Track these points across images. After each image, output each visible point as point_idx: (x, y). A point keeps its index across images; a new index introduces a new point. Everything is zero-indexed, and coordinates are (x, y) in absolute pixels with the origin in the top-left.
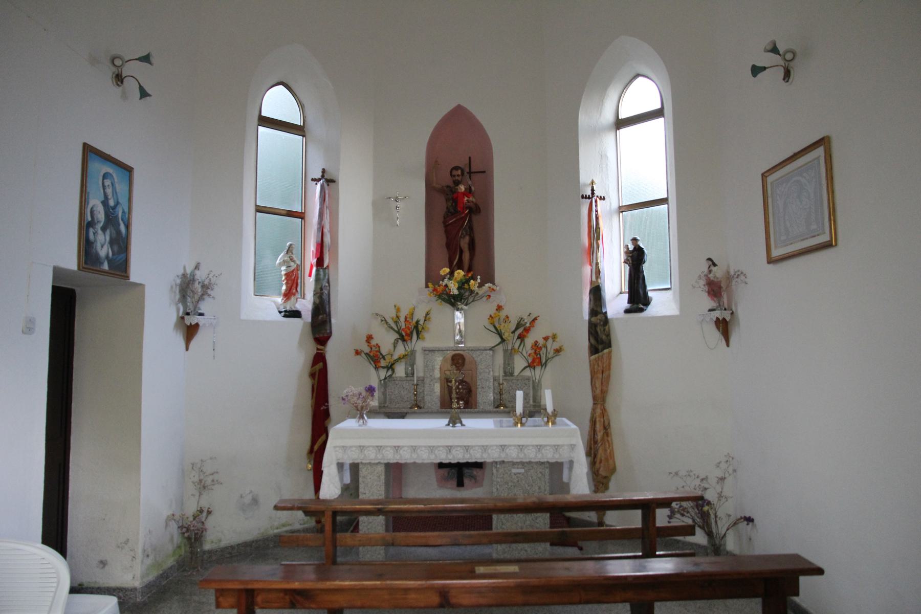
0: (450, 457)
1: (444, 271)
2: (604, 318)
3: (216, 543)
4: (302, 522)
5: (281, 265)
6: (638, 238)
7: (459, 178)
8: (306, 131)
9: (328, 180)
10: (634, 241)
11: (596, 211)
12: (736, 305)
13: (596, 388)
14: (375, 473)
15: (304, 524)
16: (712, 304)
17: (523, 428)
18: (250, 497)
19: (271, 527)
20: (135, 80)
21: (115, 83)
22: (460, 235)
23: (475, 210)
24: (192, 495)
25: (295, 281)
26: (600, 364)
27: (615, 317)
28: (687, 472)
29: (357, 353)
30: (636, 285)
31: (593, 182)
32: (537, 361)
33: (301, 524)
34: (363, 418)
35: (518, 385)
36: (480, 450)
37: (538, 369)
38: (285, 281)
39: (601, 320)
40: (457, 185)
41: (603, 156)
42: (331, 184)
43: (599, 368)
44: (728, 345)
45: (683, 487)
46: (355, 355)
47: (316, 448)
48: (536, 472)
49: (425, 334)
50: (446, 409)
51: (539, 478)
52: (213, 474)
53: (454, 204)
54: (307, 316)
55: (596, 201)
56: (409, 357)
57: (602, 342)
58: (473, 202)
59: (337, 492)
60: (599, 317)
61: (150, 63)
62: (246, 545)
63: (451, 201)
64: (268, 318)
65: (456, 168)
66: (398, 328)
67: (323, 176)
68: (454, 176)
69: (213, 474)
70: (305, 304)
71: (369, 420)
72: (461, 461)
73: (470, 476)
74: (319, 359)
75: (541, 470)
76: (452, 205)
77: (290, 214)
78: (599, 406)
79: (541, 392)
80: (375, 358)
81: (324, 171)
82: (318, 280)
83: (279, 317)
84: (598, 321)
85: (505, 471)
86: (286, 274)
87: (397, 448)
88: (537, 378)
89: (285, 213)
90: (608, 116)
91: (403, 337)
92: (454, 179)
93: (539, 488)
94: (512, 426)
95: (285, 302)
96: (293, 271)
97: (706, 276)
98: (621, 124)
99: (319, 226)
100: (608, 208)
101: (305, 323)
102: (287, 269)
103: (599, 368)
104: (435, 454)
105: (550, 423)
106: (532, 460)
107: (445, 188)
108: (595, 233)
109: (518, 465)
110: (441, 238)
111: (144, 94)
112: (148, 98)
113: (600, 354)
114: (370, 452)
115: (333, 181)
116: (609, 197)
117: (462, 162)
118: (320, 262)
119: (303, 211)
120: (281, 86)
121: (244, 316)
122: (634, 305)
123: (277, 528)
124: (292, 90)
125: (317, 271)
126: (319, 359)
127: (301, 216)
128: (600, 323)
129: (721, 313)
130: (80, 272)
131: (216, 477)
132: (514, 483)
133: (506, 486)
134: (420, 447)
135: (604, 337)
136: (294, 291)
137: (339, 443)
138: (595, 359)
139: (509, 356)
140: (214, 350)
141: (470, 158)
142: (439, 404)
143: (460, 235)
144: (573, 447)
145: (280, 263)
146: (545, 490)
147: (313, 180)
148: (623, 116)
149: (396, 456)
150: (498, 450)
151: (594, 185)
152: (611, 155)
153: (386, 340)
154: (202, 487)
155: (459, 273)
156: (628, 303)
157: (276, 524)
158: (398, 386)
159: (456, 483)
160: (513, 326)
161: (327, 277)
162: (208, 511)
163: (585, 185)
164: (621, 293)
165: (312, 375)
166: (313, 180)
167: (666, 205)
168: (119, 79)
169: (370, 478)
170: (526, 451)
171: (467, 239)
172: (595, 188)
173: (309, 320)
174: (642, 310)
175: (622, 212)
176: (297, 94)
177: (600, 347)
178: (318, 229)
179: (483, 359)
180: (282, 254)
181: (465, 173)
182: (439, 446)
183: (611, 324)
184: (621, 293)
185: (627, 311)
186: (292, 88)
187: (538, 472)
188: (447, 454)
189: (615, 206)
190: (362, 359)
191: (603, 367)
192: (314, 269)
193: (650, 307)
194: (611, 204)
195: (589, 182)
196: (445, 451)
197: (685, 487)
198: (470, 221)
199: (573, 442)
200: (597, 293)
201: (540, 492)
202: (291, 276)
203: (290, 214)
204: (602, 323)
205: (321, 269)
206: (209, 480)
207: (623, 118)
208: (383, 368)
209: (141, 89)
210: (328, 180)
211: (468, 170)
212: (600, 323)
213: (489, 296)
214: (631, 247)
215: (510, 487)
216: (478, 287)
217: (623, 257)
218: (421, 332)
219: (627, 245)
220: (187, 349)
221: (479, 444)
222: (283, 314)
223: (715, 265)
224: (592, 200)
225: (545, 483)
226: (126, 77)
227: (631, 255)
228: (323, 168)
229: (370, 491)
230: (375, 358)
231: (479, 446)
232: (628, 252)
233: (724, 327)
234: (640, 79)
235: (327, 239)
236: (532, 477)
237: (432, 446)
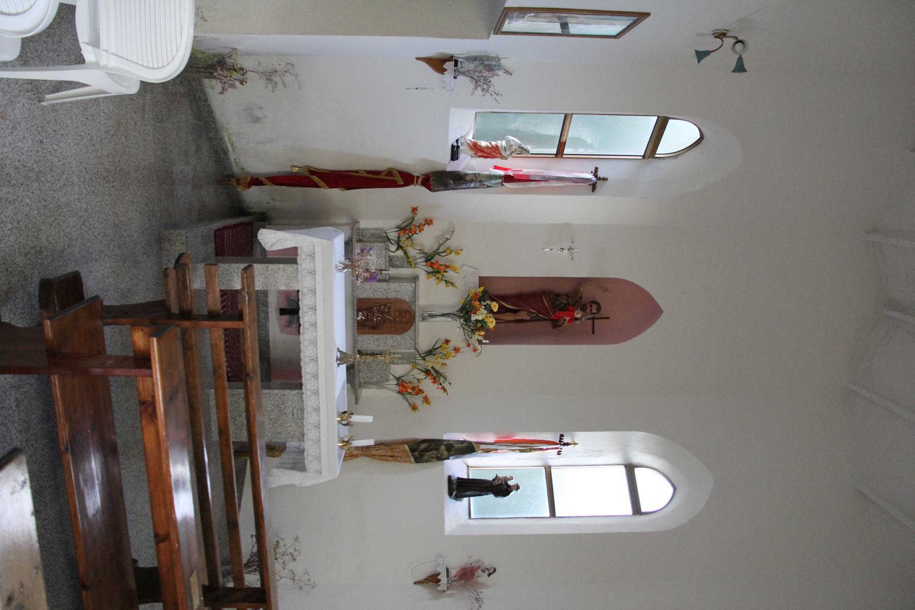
0: (308, 377)
1: (495, 306)
2: (444, 457)
3: (210, 84)
4: (237, 161)
5: (508, 141)
6: (519, 491)
7: (588, 310)
8: (648, 160)
9: (594, 185)
10: (516, 487)
11: (547, 449)
12: (451, 595)
13: (377, 450)
14: (288, 280)
15: (235, 163)
16: (453, 573)
17: (336, 422)
18: (261, 115)
19: (230, 134)
20: (718, 47)
21: (715, 32)
22: (532, 310)
23: (556, 324)
24: (259, 63)
25: (490, 156)
26: (400, 454)
27: (445, 467)
28: (299, 550)
29: (414, 210)
30: (474, 488)
31: (575, 444)
32: (405, 388)
33: (235, 160)
34: (344, 268)
35: (381, 370)
36: (314, 388)
37: (397, 388)
38: (489, 146)
39: (442, 454)
40: (581, 310)
41: (600, 452)
42: (591, 187)
43: (396, 453)
44: (415, 583)
45: (285, 545)
46: (412, 207)
47: (315, 178)
48: (295, 431)
49: (433, 280)
50: (357, 304)
51: (289, 433)
52: (283, 82)
53: (563, 305)
54: (452, 167)
55: (557, 448)
56: (409, 262)
57: (421, 456)
58: (564, 323)
59: (267, 245)
60: (446, 453)
61: (733, 71)
62: (210, 112)
63: (565, 302)
64: (450, 131)
65: (599, 308)
66: (440, 252)
67: (599, 179)
68: (591, 306)
69: (283, 82)
70: (468, 163)
71: (344, 274)
72: (303, 371)
73: (291, 321)
74: (407, 179)
75: (296, 434)
76: (562, 303)
77: (561, 146)
78: (360, 452)
79: (374, 388)
80: (408, 228)
81: (605, 179)
82: (491, 177)
83: (452, 141)
84: (441, 452)
85: (295, 402)
86: (497, 146)
87: (313, 273)
88: (387, 386)
89: (563, 139)
90: (637, 457)
91: (429, 258)
92: (588, 306)
93: (280, 433)
94: (339, 437)
95: (468, 144)
96: (500, 153)
97: (479, 567)
98: (630, 469)
99: (547, 177)
100: (549, 457)
101: (445, 165)
102: (502, 148)
103: (396, 453)
104: (309, 345)
105: (342, 444)
106: (305, 420)
107: (579, 296)
108: (528, 446)
109: (301, 414)
110: (527, 289)
111: (701, 55)
112: (697, 60)
113: (410, 454)
114: (310, 317)
115: (594, 189)
116: (560, 458)
117: (604, 312)
118: (508, 179)
119: (564, 156)
120: (699, 137)
121: (452, 110)
122: (456, 485)
123: (229, 139)
124: (694, 147)
125: (500, 177)
126: (407, 179)
127: (560, 153)
128: (440, 454)
129: (445, 584)
130: (502, 8)
131: (280, 85)
132: (284, 410)
133: (280, 403)
134: (316, 331)
135: (426, 458)
136: (479, 154)
137: (318, 250)
138: (405, 450)
139: (407, 359)
140: (417, 88)
141: (609, 318)
142: (361, 297)
143: (532, 310)
144: (319, 472)
145: (509, 141)
146: (277, 438)
147: (596, 169)
148: (637, 470)
149: (307, 324)
150: (315, 405)
151: (572, 445)
152: (600, 460)
153: (426, 239)
154: (269, 76)
155: (492, 322)
156: (458, 479)
157: (234, 138)
158: (380, 253)
159: (283, 307)
160: (437, 368)
161: (493, 185)
162: (243, 81)
163: (573, 437)
164: (468, 466)
165: (390, 172)
166: (596, 169)
167: (548, 515)
168: (721, 35)
169: (283, 276)
170: (313, 397)
171: (528, 318)
172: (569, 446)
173: (449, 169)
174: (450, 494)
175: (545, 468)
176: (690, 152)
177: (417, 454)
178: (544, 177)
179: (406, 340)
180: (519, 142)
181: (593, 316)
182: (317, 349)
183: (440, 462)
184: (468, 466)
185: (450, 478)
186: (696, 147)
187: (294, 432)
188: (310, 357)
189: (551, 463)
190: (408, 213)
191: (397, 456)
192: (502, 173)
193: (454, 501)
194: (554, 459)
195: (576, 441)
196: (312, 355)
197: (285, 547)
198: (544, 320)
199: (324, 473)
200: (468, 449)
201: (275, 433)
202: (495, 152)
203: (561, 146)
204: (439, 455)
205: (502, 181)
206: (276, 78)
207: (635, 470)
208: (399, 237)
209: (706, 54)
210: (594, 185)
211: (595, 317)
212: (440, 454)
213: (468, 346)
214: (510, 483)
215: (280, 406)
216: (478, 339)
217: (501, 475)
218: (435, 276)
219: (512, 479)
220: (417, 59)
221: (321, 436)
222: (455, 144)
223: (489, 575)
224: (558, 444)
225: (284, 438)
226: (722, 40)
227: (503, 483)
228: (609, 178)
229: (269, 275)
230: (408, 228)
231: (318, 387)
232: (506, 479)
233: (433, 579)
234: (671, 490)
235: (532, 185)
236: (289, 426)
237: (319, 410)
